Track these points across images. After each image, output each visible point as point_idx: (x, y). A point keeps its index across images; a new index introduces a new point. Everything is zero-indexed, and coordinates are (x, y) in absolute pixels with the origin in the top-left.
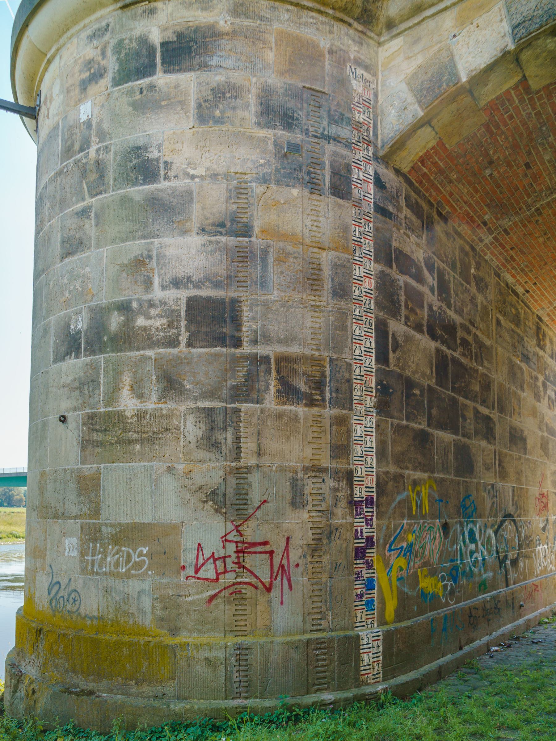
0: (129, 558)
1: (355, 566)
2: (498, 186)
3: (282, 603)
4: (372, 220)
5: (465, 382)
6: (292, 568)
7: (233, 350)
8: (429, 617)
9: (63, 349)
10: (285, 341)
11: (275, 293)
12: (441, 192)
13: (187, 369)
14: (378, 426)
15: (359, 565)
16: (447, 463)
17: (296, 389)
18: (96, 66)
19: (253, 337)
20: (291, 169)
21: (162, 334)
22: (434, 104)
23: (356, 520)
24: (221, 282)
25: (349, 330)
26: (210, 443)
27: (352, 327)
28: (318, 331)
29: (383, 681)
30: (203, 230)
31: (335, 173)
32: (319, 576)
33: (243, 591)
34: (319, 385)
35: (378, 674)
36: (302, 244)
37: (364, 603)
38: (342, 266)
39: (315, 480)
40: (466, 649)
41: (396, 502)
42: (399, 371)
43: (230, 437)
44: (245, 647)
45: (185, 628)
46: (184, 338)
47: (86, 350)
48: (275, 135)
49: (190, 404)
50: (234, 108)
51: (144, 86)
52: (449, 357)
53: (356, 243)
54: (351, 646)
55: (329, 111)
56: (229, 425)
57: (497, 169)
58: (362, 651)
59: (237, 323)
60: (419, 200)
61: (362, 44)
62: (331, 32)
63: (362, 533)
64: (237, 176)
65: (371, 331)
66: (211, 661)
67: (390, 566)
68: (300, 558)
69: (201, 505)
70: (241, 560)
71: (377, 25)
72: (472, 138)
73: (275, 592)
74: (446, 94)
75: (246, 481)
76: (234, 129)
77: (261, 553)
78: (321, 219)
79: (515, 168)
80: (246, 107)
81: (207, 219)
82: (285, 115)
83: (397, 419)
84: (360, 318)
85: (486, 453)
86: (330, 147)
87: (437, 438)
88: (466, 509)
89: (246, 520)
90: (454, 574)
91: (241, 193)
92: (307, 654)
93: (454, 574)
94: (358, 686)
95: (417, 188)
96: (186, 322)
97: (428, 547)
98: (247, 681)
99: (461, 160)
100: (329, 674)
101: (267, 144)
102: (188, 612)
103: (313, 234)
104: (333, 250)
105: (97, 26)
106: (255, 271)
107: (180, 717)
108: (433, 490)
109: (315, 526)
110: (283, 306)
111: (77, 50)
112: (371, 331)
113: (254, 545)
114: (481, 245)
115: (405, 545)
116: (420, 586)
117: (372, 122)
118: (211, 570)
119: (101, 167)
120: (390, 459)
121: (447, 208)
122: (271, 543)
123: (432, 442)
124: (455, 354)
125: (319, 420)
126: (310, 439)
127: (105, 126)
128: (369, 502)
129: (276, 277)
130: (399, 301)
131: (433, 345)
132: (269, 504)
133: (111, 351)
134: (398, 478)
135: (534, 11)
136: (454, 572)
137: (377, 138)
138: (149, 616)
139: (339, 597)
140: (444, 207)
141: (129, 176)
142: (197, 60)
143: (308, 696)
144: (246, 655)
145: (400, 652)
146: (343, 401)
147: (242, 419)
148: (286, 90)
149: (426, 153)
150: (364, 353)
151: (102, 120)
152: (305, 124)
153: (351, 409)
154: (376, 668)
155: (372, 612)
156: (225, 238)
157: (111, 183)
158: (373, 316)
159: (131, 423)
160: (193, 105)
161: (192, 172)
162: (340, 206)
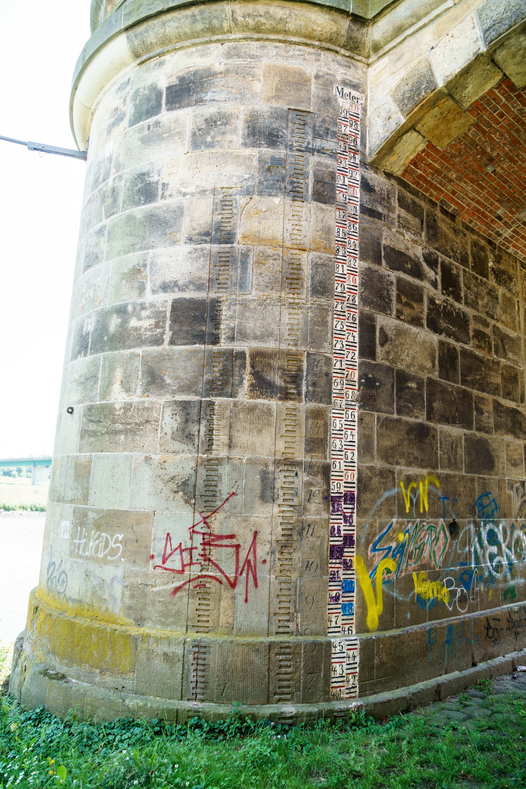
0: (107, 542)
1: (330, 565)
2: (505, 181)
3: (246, 601)
4: (358, 221)
5: (481, 375)
6: (259, 565)
7: (210, 347)
8: (427, 626)
9: (77, 348)
10: (262, 337)
11: (254, 293)
12: (443, 192)
13: (169, 365)
14: (361, 419)
15: (335, 565)
16: (455, 458)
17: (270, 383)
18: (119, 112)
19: (229, 334)
20: (274, 180)
21: (149, 333)
22: (415, 110)
23: (332, 517)
24: (203, 284)
25: (330, 324)
26: (185, 435)
27: (332, 322)
28: (295, 328)
29: (360, 696)
30: (191, 240)
31: (318, 181)
32: (288, 574)
33: (208, 585)
34: (296, 379)
35: (353, 688)
36: (282, 247)
37: (340, 606)
38: (323, 265)
39: (288, 474)
40: (482, 666)
41: (383, 499)
42: (389, 364)
43: (203, 429)
44: (203, 644)
45: (150, 618)
46: (167, 337)
47: (91, 349)
48: (259, 153)
49: (169, 397)
50: (224, 133)
51: (151, 123)
52: (458, 349)
53: (340, 243)
54: (320, 655)
55: (315, 126)
56: (203, 418)
57: (499, 165)
58: (333, 660)
59: (216, 322)
60: (417, 200)
61: (350, 67)
62: (318, 60)
63: (339, 530)
64: (224, 190)
65: (355, 325)
66: (169, 657)
67: (373, 568)
68: (268, 554)
69: (172, 495)
70: (207, 552)
71: (364, 49)
72: (463, 138)
73: (240, 588)
74: (425, 100)
75: (216, 472)
76: (222, 151)
77: (227, 546)
78: (303, 223)
79: (520, 162)
80: (235, 131)
81: (194, 230)
82: (271, 134)
83: (386, 412)
84: (342, 314)
85: (511, 448)
86: (314, 159)
87: (441, 432)
88: (484, 507)
89: (214, 512)
90: (465, 578)
91: (226, 205)
92: (269, 658)
93: (465, 578)
94: (328, 700)
95: (414, 189)
96: (170, 322)
97: (427, 549)
98: (204, 683)
99: (457, 160)
100: (293, 683)
101: (252, 161)
102: (153, 603)
103: (294, 237)
104: (314, 250)
105: (122, 81)
106: (235, 273)
107: (133, 714)
108: (435, 486)
109: (286, 521)
110: (260, 305)
111: (110, 101)
112: (355, 325)
113: (221, 537)
114: (500, 239)
115: (394, 545)
116: (416, 591)
117: (360, 133)
118: (177, 561)
119: (115, 193)
120: (375, 453)
121: (453, 206)
122: (238, 537)
123: (433, 436)
124: (466, 347)
125: (294, 413)
126: (283, 432)
127: (121, 159)
128: (349, 498)
129: (254, 278)
130: (389, 296)
131: (435, 338)
132: (238, 497)
133: (110, 350)
134: (387, 475)
135: (503, 14)
136: (466, 577)
137: (365, 147)
138: (119, 603)
139: (310, 599)
140: (449, 205)
141: (134, 198)
142: (194, 97)
143: (268, 705)
144: (205, 653)
145: (380, 665)
146: (321, 394)
147: (216, 412)
148: (272, 114)
149: (417, 156)
150: (345, 347)
151: (119, 155)
152: (290, 141)
153: (330, 403)
154: (351, 681)
155: (350, 617)
156: (209, 245)
157: (121, 205)
158: (357, 311)
159: (119, 415)
160: (188, 135)
161: (184, 190)
162: (322, 210)
